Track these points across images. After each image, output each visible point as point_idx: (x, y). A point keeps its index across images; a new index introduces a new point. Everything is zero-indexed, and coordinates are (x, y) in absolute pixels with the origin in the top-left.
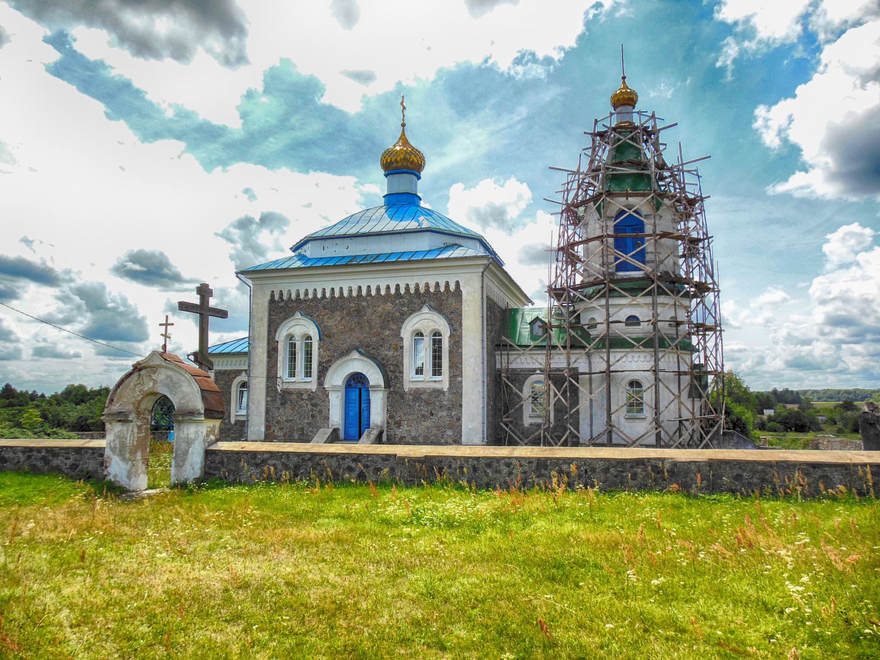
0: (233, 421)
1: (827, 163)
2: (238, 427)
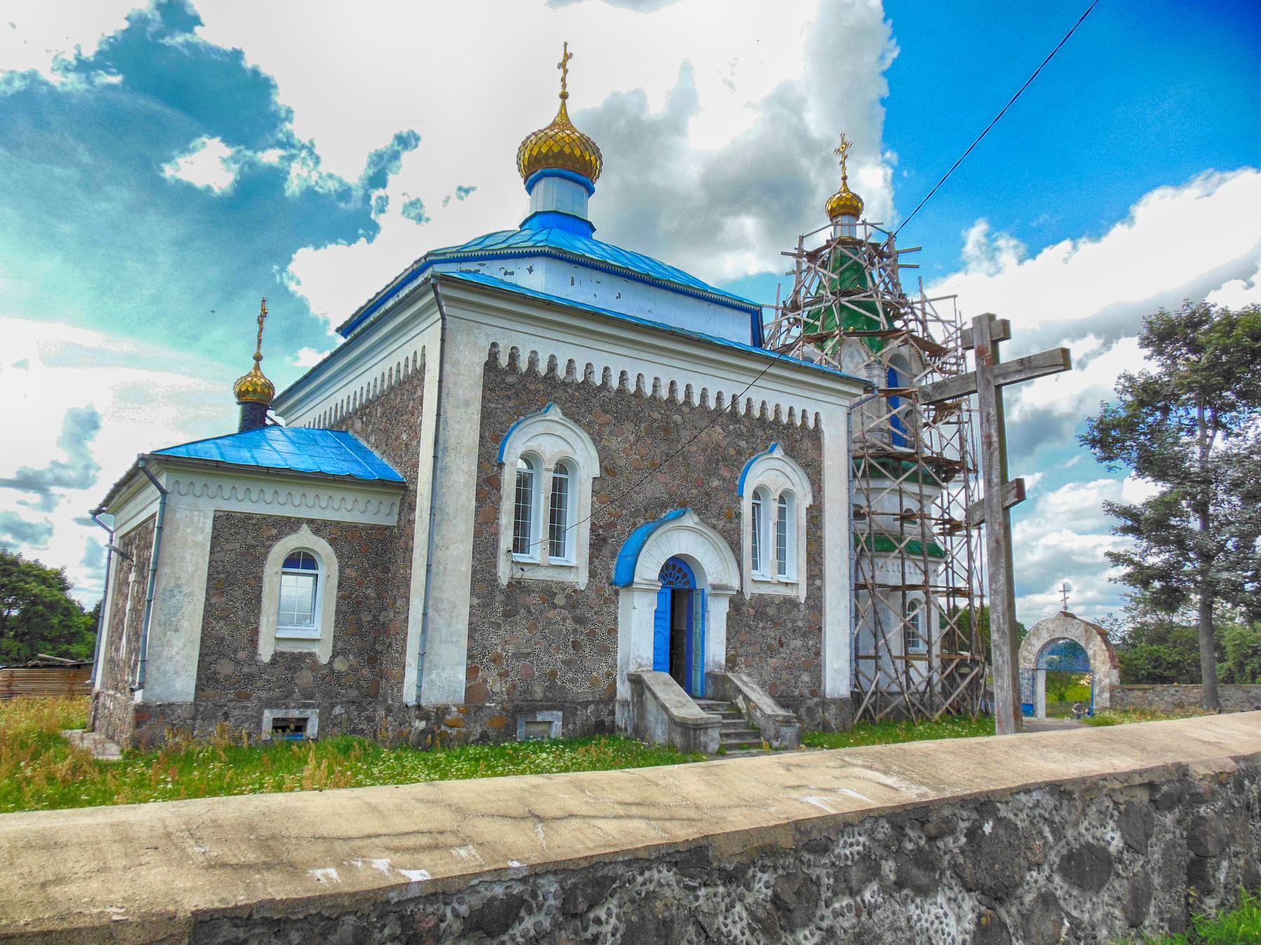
0: (265, 652)
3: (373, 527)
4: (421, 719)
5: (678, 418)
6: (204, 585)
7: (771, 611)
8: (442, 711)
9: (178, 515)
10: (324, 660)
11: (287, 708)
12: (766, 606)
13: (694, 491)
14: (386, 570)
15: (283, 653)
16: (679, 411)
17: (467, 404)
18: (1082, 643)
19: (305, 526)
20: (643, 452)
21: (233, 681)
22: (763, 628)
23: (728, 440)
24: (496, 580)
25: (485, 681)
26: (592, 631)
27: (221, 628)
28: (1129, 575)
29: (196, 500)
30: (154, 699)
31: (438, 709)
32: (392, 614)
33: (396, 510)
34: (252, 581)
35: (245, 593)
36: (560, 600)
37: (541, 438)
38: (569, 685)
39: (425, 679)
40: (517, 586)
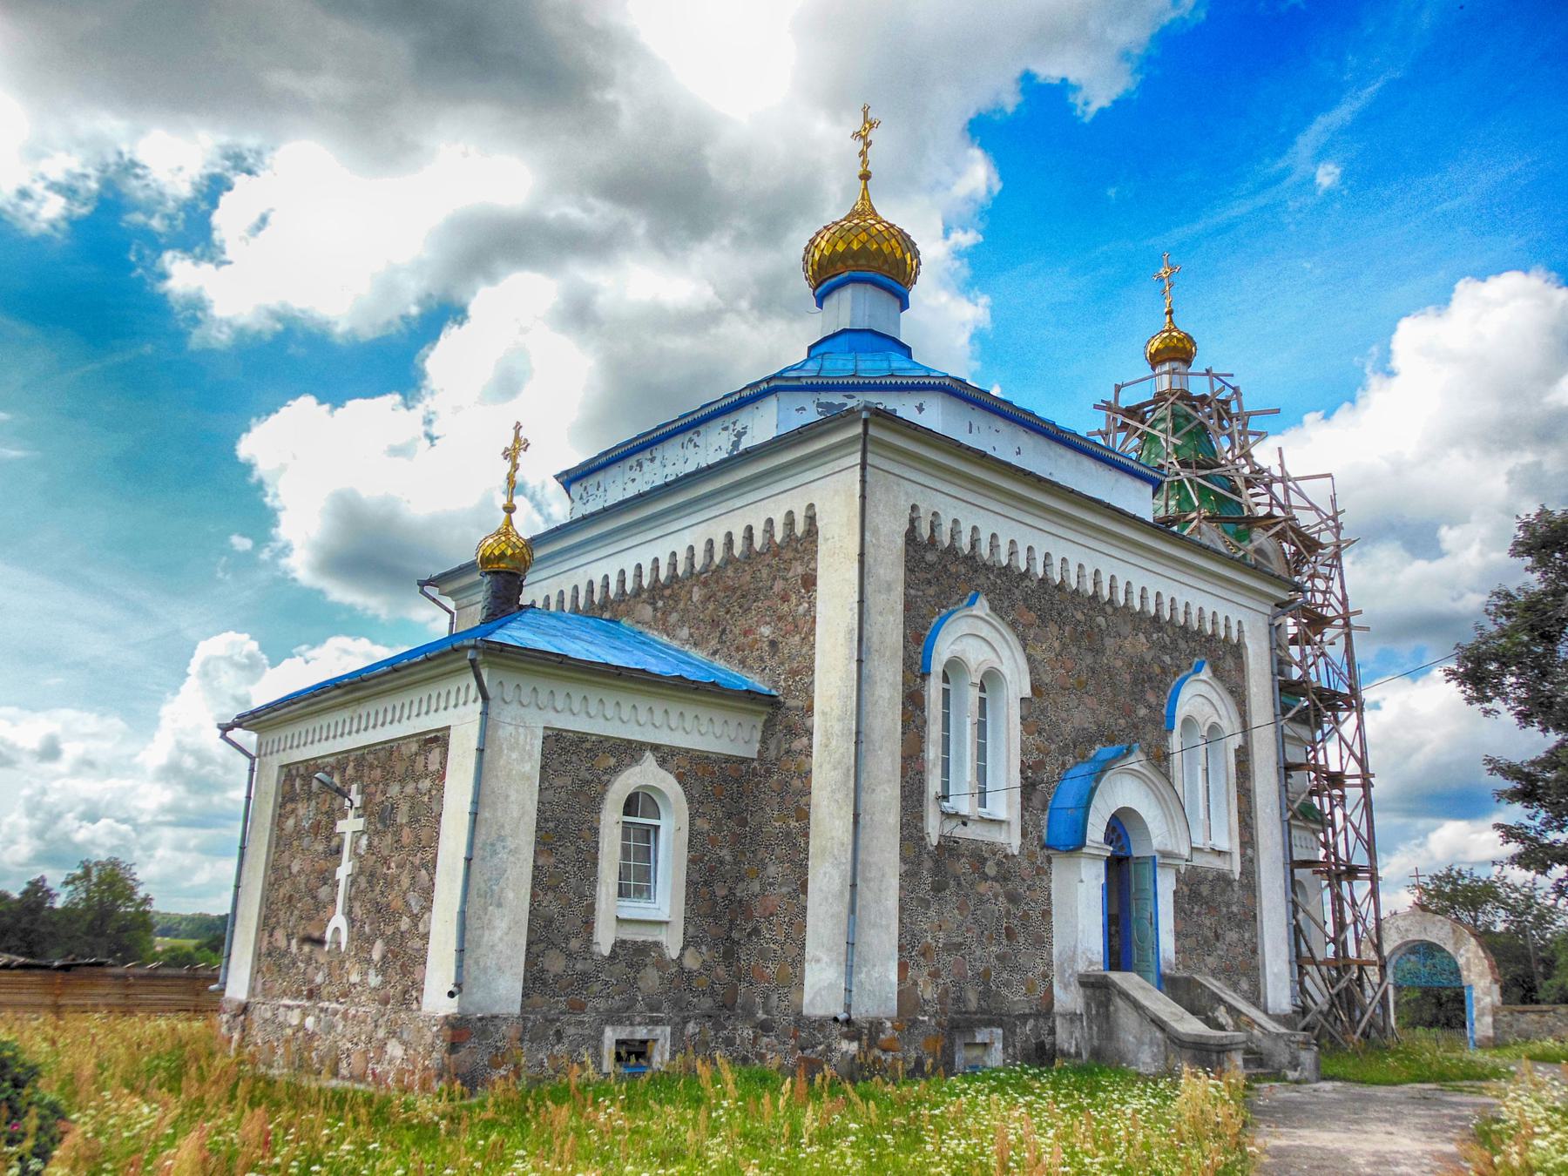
0: (605, 938)
1: (1353, 563)
2: (620, 968)
3: (728, 759)
4: (851, 1038)
5: (1101, 620)
6: (533, 838)
7: (1205, 890)
8: (876, 1026)
9: (500, 732)
10: (673, 952)
11: (632, 1024)
12: (1200, 883)
13: (1122, 721)
14: (743, 823)
15: (624, 942)
16: (1103, 612)
17: (889, 588)
18: (1449, 948)
19: (648, 753)
20: (1069, 665)
21: (564, 983)
22: (1199, 914)
23: (1152, 652)
24: (923, 839)
25: (915, 984)
26: (1026, 914)
27: (552, 906)
28: (1520, 856)
29: (522, 711)
30: (472, 1009)
31: (871, 1023)
32: (756, 887)
33: (758, 735)
34: (586, 834)
35: (579, 851)
36: (991, 869)
37: (965, 640)
38: (1004, 991)
39: (855, 980)
40: (949, 847)
